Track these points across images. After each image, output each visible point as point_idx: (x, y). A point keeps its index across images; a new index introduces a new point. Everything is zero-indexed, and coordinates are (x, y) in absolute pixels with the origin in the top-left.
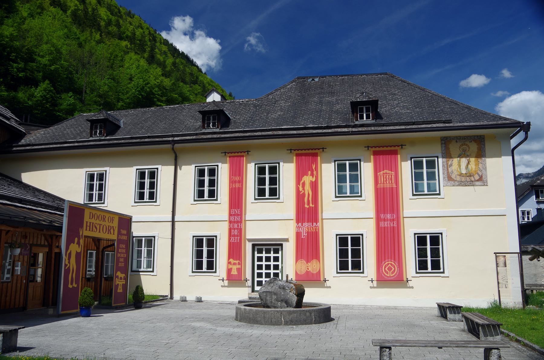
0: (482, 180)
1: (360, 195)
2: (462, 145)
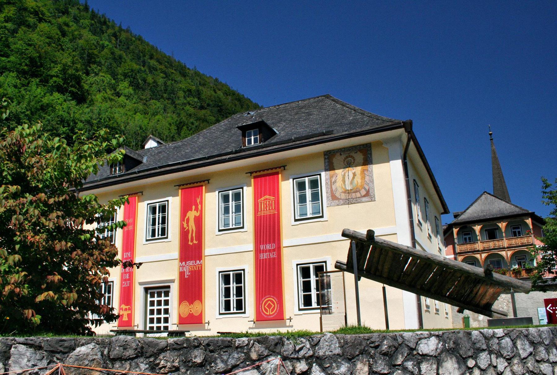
0: (369, 195)
1: (321, 215)
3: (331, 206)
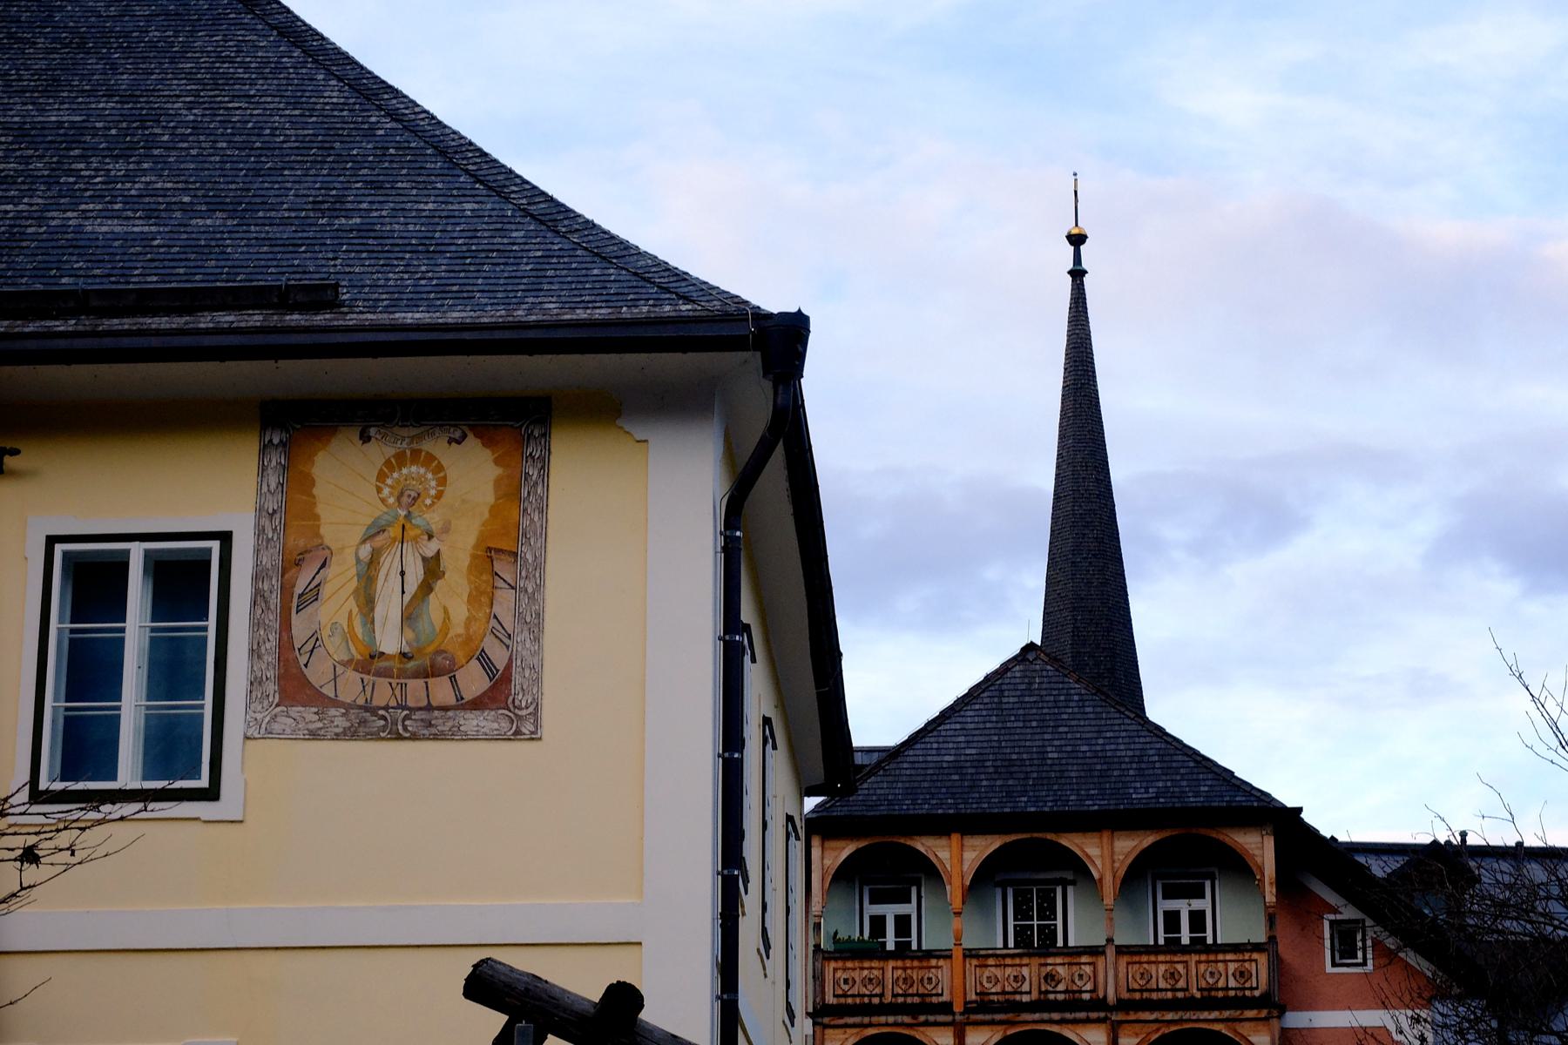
0: (504, 699)
2: (401, 459)
3: (269, 734)
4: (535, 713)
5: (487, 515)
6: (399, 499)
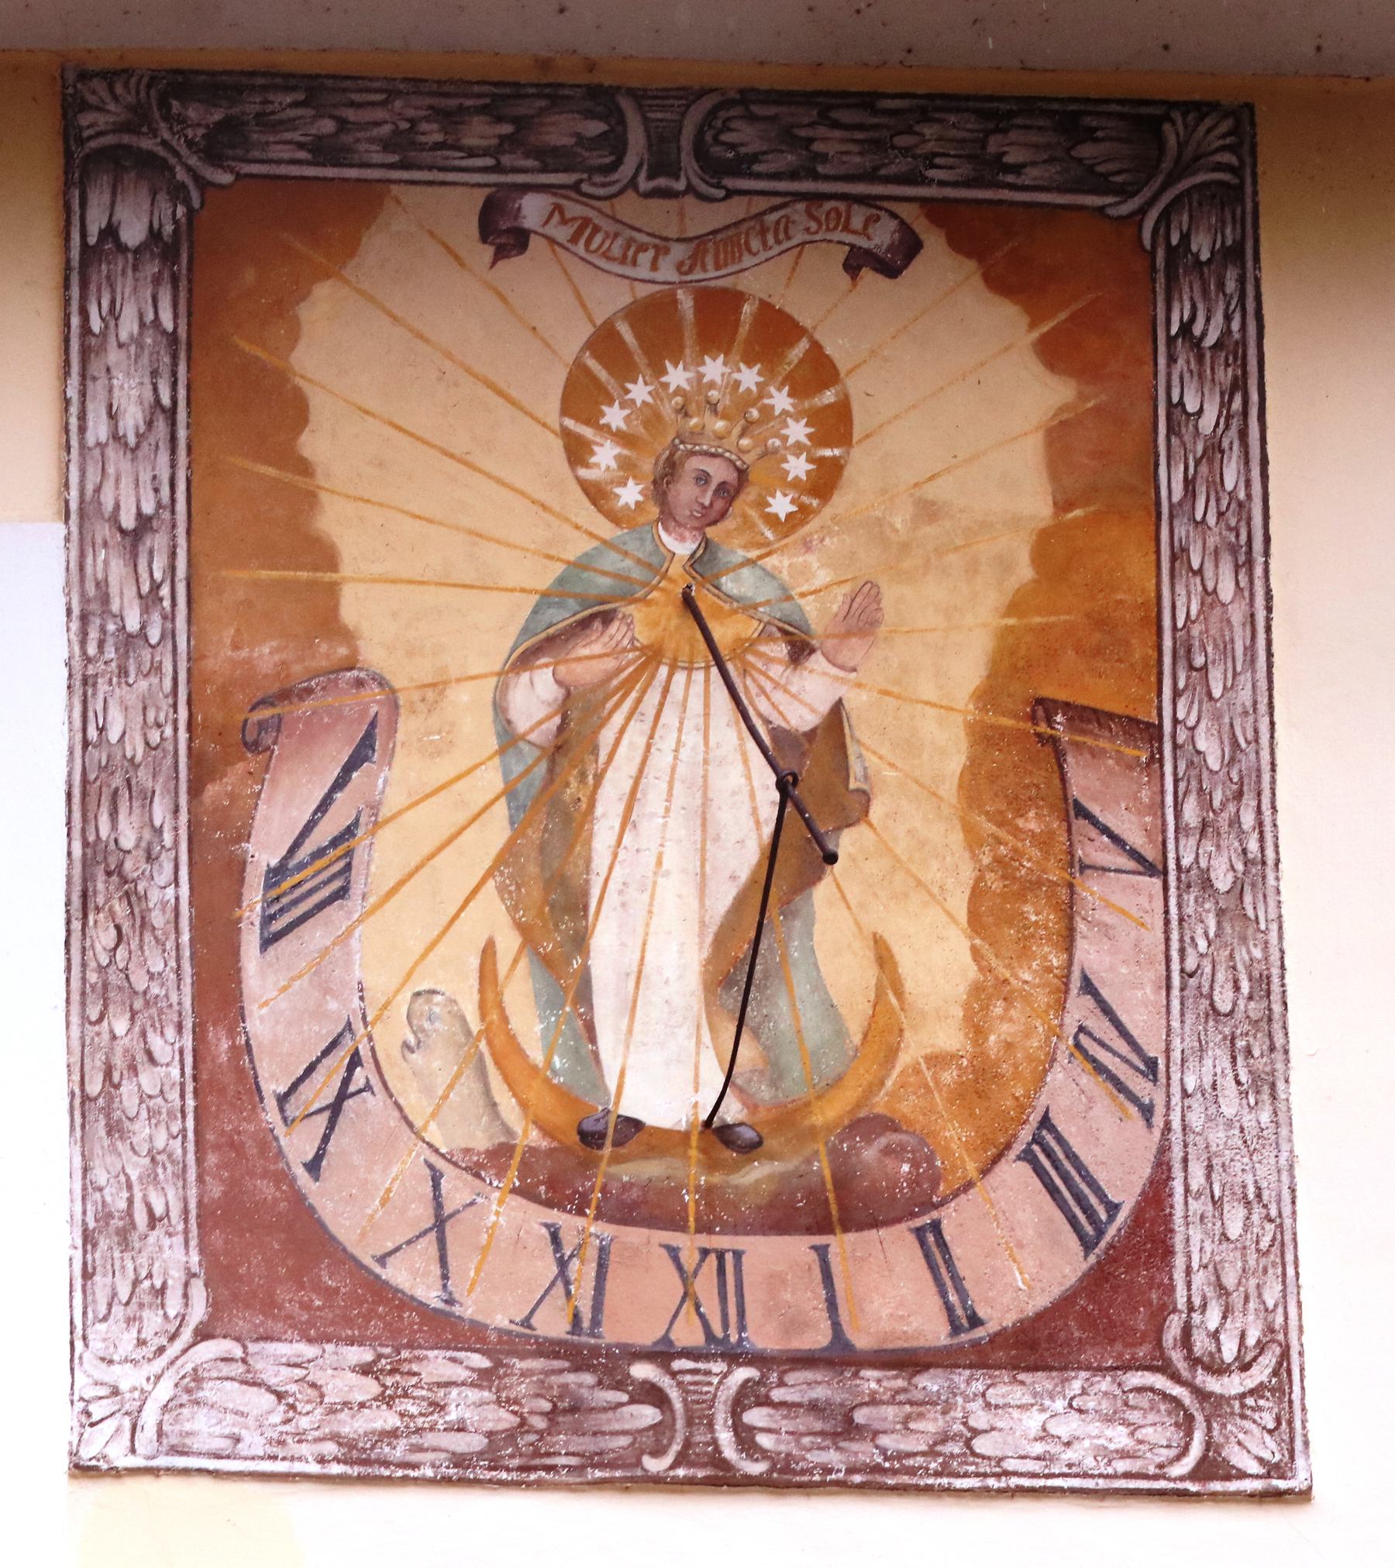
0: (1141, 1314)
2: (657, 332)
3: (173, 1461)
4: (1282, 1384)
5: (1025, 572)
6: (661, 486)
